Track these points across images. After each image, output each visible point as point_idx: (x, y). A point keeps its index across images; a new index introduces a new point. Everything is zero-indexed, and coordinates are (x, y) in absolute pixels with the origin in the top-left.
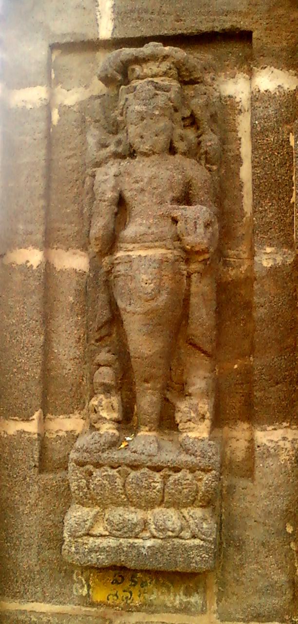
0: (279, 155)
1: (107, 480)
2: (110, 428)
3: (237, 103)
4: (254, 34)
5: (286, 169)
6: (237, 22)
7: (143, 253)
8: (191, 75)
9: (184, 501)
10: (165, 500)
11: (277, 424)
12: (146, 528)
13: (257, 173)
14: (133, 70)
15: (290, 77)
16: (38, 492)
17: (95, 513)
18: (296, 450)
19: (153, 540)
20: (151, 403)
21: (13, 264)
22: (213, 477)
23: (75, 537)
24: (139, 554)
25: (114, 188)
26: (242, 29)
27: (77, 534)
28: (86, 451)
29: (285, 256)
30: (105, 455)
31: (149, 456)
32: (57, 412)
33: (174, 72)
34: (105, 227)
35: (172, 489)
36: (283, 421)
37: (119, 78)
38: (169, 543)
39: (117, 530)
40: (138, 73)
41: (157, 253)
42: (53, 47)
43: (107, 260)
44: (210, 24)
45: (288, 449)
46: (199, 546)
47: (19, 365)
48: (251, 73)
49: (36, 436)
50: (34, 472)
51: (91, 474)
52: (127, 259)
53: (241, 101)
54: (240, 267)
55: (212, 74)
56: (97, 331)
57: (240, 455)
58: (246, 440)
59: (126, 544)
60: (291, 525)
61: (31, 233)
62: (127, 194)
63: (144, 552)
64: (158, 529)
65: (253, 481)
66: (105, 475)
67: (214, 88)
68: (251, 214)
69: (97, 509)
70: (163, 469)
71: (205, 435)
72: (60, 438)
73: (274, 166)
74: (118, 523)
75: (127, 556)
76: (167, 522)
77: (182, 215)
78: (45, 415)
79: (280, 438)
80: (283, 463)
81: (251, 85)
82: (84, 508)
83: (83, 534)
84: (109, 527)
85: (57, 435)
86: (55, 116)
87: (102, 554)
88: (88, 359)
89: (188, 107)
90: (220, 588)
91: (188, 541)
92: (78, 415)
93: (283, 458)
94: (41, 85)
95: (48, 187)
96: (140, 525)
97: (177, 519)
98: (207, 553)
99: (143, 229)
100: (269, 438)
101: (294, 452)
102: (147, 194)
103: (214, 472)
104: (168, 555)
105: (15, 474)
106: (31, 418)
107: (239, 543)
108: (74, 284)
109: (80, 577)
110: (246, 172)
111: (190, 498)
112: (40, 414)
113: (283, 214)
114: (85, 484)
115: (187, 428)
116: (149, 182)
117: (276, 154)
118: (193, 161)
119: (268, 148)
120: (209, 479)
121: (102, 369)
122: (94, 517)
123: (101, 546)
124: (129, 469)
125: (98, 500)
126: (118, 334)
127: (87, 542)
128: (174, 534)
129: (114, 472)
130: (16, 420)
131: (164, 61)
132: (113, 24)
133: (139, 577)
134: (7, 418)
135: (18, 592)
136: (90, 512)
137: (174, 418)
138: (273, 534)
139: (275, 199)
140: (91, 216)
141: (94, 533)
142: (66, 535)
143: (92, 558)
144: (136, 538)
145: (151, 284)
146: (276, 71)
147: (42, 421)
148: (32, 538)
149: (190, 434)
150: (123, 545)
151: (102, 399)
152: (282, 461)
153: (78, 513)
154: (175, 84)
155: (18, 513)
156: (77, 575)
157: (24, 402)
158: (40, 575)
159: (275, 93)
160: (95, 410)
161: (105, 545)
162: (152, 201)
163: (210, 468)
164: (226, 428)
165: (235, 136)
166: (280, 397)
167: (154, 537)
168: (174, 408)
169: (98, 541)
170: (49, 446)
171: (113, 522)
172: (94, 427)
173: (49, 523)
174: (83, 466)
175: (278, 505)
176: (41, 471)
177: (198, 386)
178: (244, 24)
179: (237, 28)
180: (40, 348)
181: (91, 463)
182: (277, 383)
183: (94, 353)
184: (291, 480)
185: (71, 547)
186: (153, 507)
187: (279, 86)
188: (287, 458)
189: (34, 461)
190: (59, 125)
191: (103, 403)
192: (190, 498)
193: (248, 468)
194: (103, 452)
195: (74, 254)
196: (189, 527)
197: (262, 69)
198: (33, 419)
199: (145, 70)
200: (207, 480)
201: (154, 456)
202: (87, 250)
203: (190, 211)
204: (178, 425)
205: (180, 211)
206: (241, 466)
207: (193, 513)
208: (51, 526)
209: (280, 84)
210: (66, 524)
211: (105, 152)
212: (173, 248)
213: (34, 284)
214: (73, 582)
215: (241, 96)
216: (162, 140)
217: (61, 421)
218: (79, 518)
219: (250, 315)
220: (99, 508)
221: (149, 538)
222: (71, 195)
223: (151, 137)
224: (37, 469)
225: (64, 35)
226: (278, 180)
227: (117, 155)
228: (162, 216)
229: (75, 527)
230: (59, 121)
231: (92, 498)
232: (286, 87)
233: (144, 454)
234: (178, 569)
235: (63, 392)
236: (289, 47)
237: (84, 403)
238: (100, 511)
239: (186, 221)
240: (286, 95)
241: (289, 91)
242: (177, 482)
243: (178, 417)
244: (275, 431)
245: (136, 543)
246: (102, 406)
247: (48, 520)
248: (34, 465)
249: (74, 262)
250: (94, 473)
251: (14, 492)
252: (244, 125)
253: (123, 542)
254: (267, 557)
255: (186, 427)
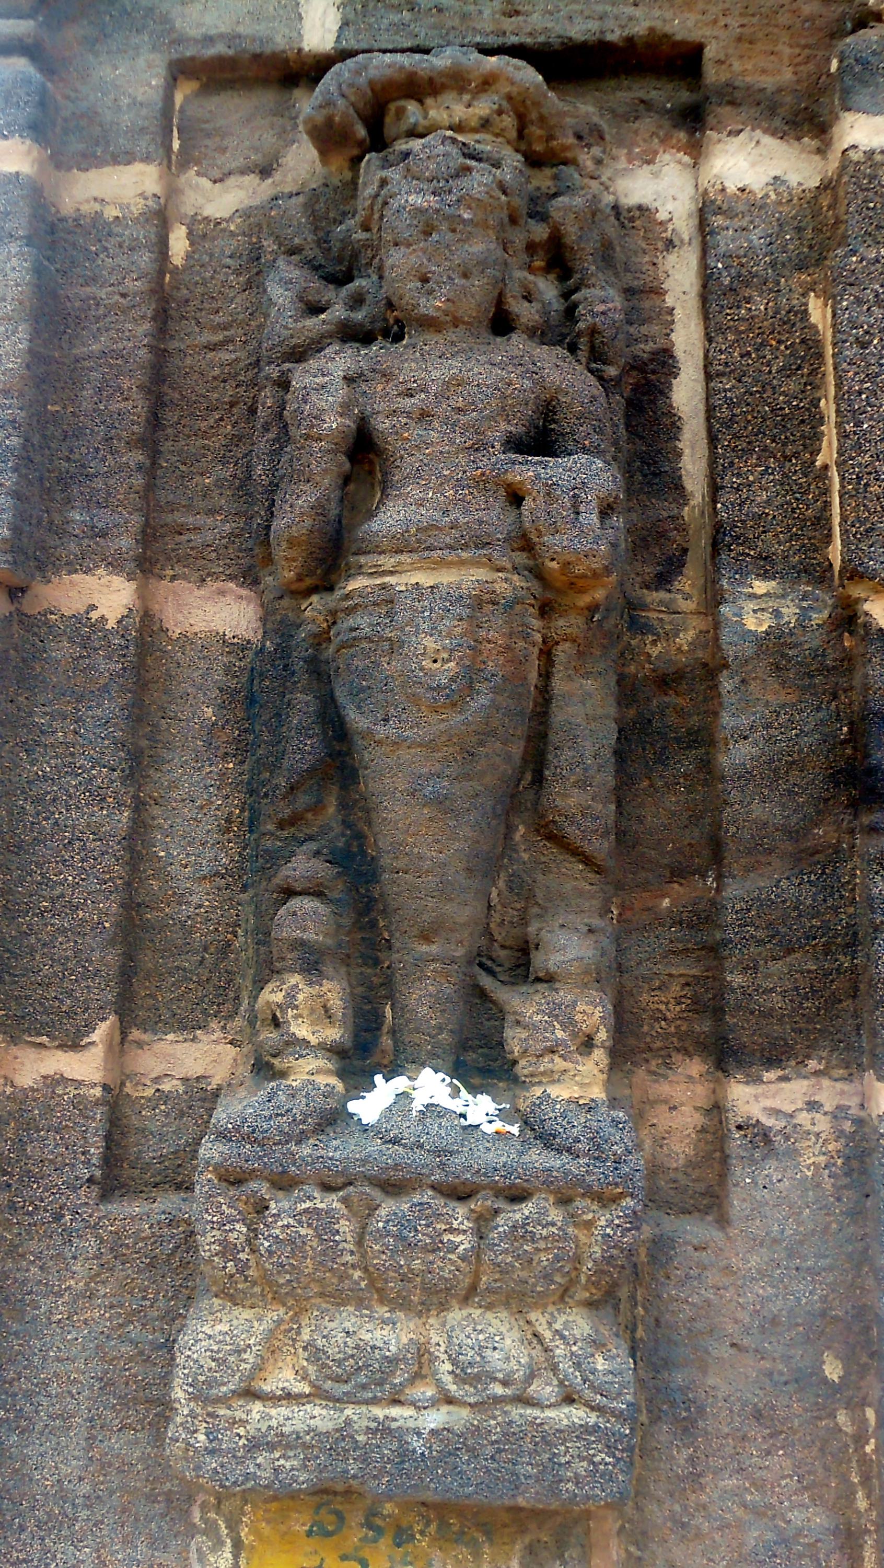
0: (782, 347)
1: (310, 1225)
2: (319, 1071)
3: (661, 223)
4: (707, 50)
5: (803, 381)
6: (665, 21)
7: (425, 579)
8: (551, 137)
9: (539, 1289)
10: (482, 1286)
11: (793, 1063)
12: (424, 1372)
13: (725, 391)
14: (401, 112)
15: (803, 156)
16: (96, 1257)
17: (272, 1326)
18: (846, 1137)
19: (445, 1409)
20: (438, 1000)
21: (52, 613)
22: (626, 1216)
23: (207, 1400)
24: (404, 1454)
25: (345, 408)
26: (678, 37)
27: (214, 1391)
28: (249, 1138)
29: (805, 604)
30: (306, 1150)
31: (438, 1152)
32: (158, 1024)
33: (508, 122)
34: (319, 509)
35: (506, 1252)
36: (808, 1057)
37: (361, 132)
38: (495, 1418)
39: (338, 1379)
40: (412, 120)
41: (470, 577)
42: (181, 70)
43: (315, 607)
44: (594, 26)
45: (823, 1136)
46: (586, 1429)
47: (58, 891)
48: (696, 151)
49: (98, 1092)
50: (86, 1196)
51: (262, 1208)
52: (385, 595)
53: (671, 220)
54: (677, 635)
55: (596, 151)
56: (284, 798)
57: (681, 1149)
58: (696, 1109)
59: (365, 1423)
60: (837, 1357)
61: (103, 534)
62: (382, 424)
63: (417, 1444)
64: (461, 1377)
65: (723, 1222)
66: (306, 1211)
67: (602, 184)
68: (703, 496)
69: (274, 1314)
70: (477, 1192)
71: (598, 1093)
72: (164, 1097)
73: (770, 372)
74: (341, 1356)
75: (365, 1459)
76: (488, 1353)
77: (538, 476)
78: (124, 1034)
79: (800, 1105)
80: (809, 1174)
81: (696, 179)
82: (237, 1311)
83: (234, 1392)
84: (312, 1369)
85: (158, 1090)
86: (179, 244)
87: (291, 1454)
88: (255, 873)
89: (543, 217)
90: (632, 1549)
91: (551, 1413)
92: (218, 1034)
93: (808, 1162)
94: (147, 159)
95: (155, 421)
96: (406, 1364)
97: (517, 1344)
98: (610, 1449)
99: (426, 514)
100: (769, 1103)
101: (839, 1145)
102: (436, 424)
103: (628, 1202)
104: (492, 1458)
105: (32, 1203)
106: (86, 1040)
107: (688, 1409)
108: (218, 676)
109: (212, 1515)
110: (686, 393)
111: (558, 1279)
112: (112, 1027)
113: (798, 495)
114: (242, 1238)
115: (543, 1074)
116: (441, 396)
117: (774, 343)
118: (560, 351)
119: (750, 330)
120: (616, 1222)
121: (295, 903)
122: (268, 1340)
123: (286, 1430)
124: (377, 1194)
125: (281, 1286)
126: (344, 806)
127: (244, 1416)
128: (508, 1392)
129: (333, 1202)
130: (41, 1045)
131: (486, 91)
132: (339, 16)
133: (389, 1516)
134: (14, 1040)
135: (24, 1561)
136: (256, 1324)
137: (501, 1044)
138: (786, 1383)
139: (775, 457)
140: (273, 488)
141: (267, 1388)
142: (178, 1393)
143: (259, 1466)
144: (396, 1402)
145: (449, 660)
146: (767, 140)
147: (117, 1049)
148: (73, 1397)
149: (554, 1091)
150: (356, 1427)
151: (296, 986)
152: (809, 1169)
153: (219, 1328)
154: (512, 160)
155: (35, 1318)
156: (204, 1507)
157: (70, 994)
158: (88, 1507)
159: (767, 196)
160: (274, 1017)
161: (300, 1427)
162: (452, 442)
163: (620, 1190)
164: (641, 1073)
165: (658, 303)
166: (797, 989)
167: (450, 1401)
168: (499, 1014)
169: (279, 1413)
170: (135, 1121)
171: (325, 1353)
172: (270, 1066)
173: (127, 1349)
174: (238, 1182)
175: (799, 1299)
176: (105, 1196)
177: (571, 954)
178: (682, 25)
179: (666, 36)
180: (119, 843)
181: (259, 1177)
182: (790, 951)
183: (274, 859)
184: (834, 1226)
185: (196, 1431)
186: (443, 1307)
187: (776, 178)
188: (822, 1159)
189: (87, 1163)
190: (187, 268)
191: (301, 997)
192: (558, 1279)
193: (701, 1187)
194: (299, 1142)
195: (222, 593)
196: (554, 1368)
197: (730, 134)
198: (92, 1043)
199: (432, 113)
200: (610, 1223)
201: (452, 1153)
202: (256, 582)
203: (558, 470)
204: (515, 1062)
205: (526, 471)
206: (683, 1180)
207: (566, 1323)
208: (131, 1359)
209: (778, 173)
210: (180, 1360)
211: (314, 324)
212: (509, 566)
213: (106, 666)
214: (192, 1531)
215: (670, 207)
216: (476, 294)
217: (170, 1049)
218: (220, 1342)
219: (707, 765)
220: (282, 1311)
221: (434, 1403)
222: (216, 443)
223: (449, 278)
224: (95, 1190)
225: (209, 40)
226: (782, 409)
227: (355, 335)
228: (481, 483)
229: (210, 1369)
230: (188, 256)
231: (267, 1279)
232: (793, 179)
233: (421, 1146)
234: (521, 1501)
235: (178, 968)
236: (798, 81)
237: (237, 998)
238: (286, 1317)
239: (548, 494)
240: (795, 201)
241: (804, 191)
242: (521, 1232)
243: (515, 1039)
244: (783, 1085)
245: (395, 1420)
246: (296, 1007)
247: (123, 1339)
248: (87, 1176)
249: (218, 614)
250: (273, 1205)
251: (23, 1256)
252: (680, 277)
253: (355, 1418)
254: (768, 1453)
255: (542, 1069)
